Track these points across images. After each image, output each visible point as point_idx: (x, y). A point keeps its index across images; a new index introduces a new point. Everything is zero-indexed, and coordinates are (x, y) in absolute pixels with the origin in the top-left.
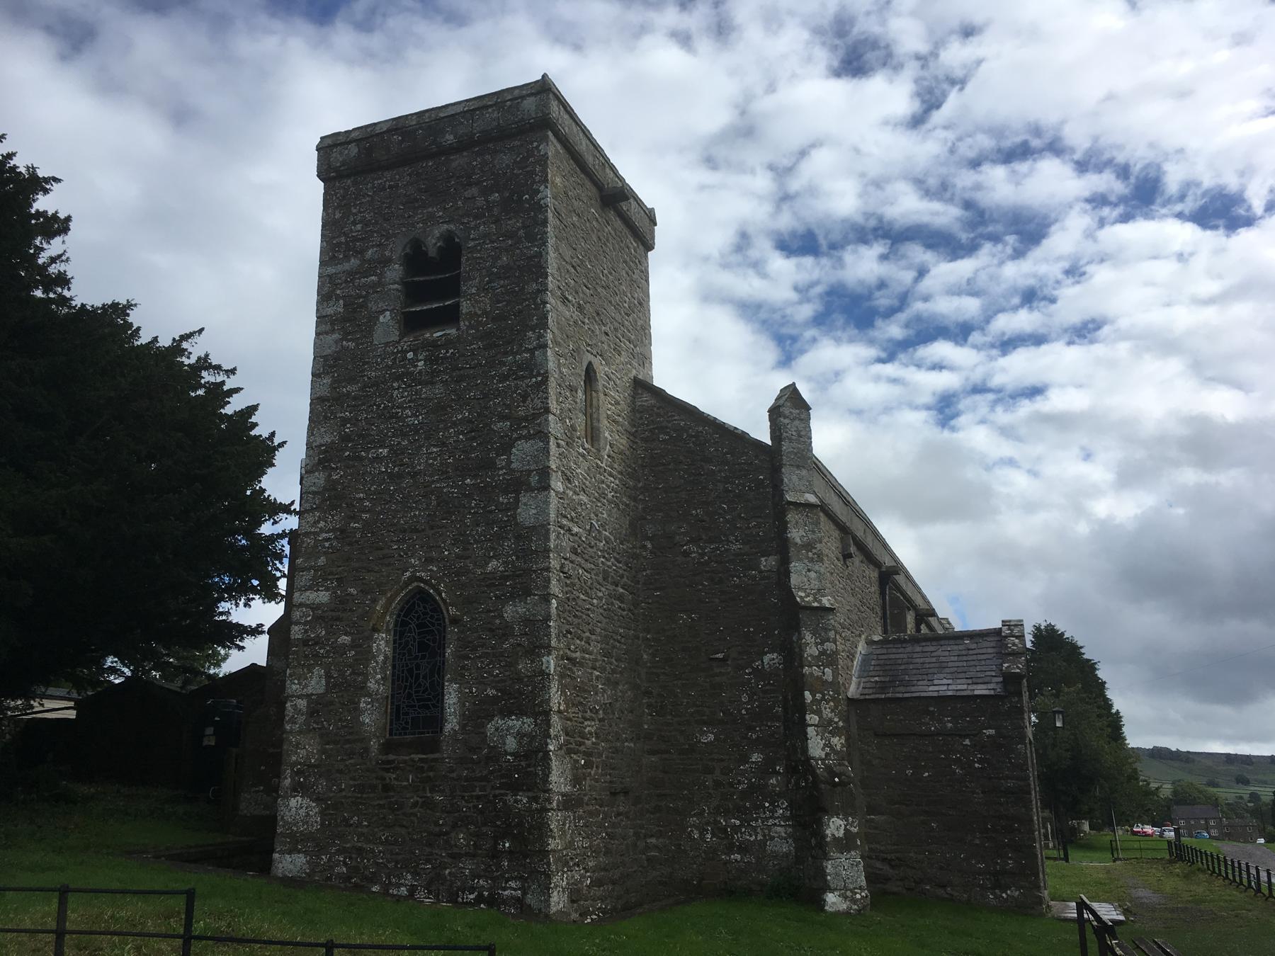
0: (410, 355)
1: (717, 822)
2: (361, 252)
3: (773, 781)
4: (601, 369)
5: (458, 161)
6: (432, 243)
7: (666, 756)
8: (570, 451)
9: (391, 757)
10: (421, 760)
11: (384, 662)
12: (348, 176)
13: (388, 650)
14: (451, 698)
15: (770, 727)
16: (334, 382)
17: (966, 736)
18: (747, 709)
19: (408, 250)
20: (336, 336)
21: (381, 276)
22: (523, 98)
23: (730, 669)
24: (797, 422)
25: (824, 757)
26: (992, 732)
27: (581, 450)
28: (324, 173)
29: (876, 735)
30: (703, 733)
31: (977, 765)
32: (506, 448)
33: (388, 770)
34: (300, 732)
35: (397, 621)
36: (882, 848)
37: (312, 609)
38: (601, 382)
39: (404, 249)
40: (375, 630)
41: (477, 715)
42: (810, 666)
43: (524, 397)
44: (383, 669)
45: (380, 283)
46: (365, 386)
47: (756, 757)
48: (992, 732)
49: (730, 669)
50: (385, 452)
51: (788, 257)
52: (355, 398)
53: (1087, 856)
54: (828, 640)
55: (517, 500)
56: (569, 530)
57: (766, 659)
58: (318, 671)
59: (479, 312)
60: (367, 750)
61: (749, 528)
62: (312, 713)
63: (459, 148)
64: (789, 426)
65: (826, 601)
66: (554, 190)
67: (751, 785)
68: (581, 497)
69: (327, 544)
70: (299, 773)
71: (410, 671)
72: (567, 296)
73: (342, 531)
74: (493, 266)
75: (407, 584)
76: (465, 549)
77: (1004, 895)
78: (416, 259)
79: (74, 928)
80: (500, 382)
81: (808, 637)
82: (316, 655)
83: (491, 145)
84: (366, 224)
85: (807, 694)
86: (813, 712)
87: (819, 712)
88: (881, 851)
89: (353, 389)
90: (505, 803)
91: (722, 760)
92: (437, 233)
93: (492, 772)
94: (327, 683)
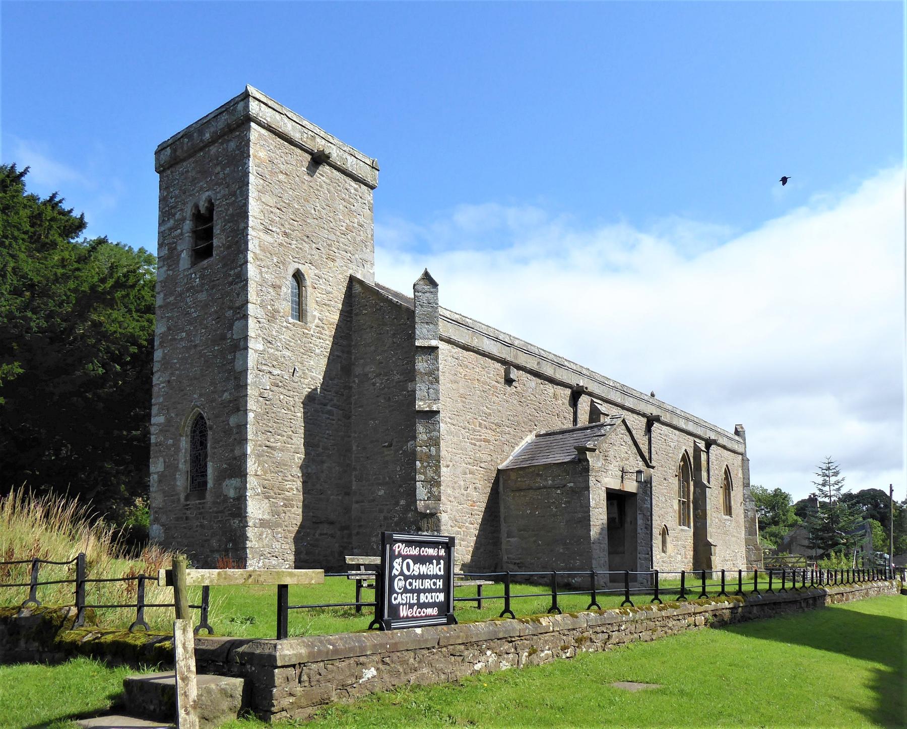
0: (193, 276)
2: (174, 215)
4: (309, 272)
5: (213, 150)
7: (362, 504)
8: (271, 325)
9: (188, 503)
10: (200, 504)
11: (185, 453)
12: (168, 168)
13: (188, 446)
14: (210, 471)
15: (409, 484)
16: (165, 295)
17: (558, 488)
18: (399, 475)
19: (193, 211)
20: (165, 268)
21: (182, 229)
22: (237, 103)
23: (392, 452)
24: (428, 295)
25: (426, 499)
26: (572, 484)
27: (285, 324)
28: (161, 169)
30: (379, 490)
31: (563, 505)
32: (231, 327)
33: (187, 509)
34: (155, 492)
35: (191, 430)
36: (514, 557)
37: (159, 426)
38: (308, 282)
39: (191, 211)
40: (181, 436)
42: (421, 447)
43: (238, 295)
44: (185, 457)
45: (182, 234)
46: (176, 297)
47: (402, 502)
48: (572, 484)
49: (392, 452)
50: (184, 334)
52: (173, 305)
54: (434, 430)
55: (235, 356)
57: (409, 444)
58: (161, 459)
59: (221, 245)
60: (179, 500)
61: (403, 365)
62: (160, 481)
63: (212, 142)
64: (421, 297)
66: (257, 160)
67: (400, 517)
68: (284, 353)
69: (163, 390)
70: (156, 512)
71: (197, 457)
72: (270, 228)
73: (169, 382)
74: (226, 215)
76: (215, 387)
77: (573, 581)
80: (229, 287)
81: (420, 428)
82: (160, 451)
83: (226, 137)
84: (176, 197)
85: (418, 463)
88: (514, 559)
89: (172, 298)
90: (230, 524)
91: (387, 505)
92: (204, 198)
93: (225, 508)
94: (165, 465)
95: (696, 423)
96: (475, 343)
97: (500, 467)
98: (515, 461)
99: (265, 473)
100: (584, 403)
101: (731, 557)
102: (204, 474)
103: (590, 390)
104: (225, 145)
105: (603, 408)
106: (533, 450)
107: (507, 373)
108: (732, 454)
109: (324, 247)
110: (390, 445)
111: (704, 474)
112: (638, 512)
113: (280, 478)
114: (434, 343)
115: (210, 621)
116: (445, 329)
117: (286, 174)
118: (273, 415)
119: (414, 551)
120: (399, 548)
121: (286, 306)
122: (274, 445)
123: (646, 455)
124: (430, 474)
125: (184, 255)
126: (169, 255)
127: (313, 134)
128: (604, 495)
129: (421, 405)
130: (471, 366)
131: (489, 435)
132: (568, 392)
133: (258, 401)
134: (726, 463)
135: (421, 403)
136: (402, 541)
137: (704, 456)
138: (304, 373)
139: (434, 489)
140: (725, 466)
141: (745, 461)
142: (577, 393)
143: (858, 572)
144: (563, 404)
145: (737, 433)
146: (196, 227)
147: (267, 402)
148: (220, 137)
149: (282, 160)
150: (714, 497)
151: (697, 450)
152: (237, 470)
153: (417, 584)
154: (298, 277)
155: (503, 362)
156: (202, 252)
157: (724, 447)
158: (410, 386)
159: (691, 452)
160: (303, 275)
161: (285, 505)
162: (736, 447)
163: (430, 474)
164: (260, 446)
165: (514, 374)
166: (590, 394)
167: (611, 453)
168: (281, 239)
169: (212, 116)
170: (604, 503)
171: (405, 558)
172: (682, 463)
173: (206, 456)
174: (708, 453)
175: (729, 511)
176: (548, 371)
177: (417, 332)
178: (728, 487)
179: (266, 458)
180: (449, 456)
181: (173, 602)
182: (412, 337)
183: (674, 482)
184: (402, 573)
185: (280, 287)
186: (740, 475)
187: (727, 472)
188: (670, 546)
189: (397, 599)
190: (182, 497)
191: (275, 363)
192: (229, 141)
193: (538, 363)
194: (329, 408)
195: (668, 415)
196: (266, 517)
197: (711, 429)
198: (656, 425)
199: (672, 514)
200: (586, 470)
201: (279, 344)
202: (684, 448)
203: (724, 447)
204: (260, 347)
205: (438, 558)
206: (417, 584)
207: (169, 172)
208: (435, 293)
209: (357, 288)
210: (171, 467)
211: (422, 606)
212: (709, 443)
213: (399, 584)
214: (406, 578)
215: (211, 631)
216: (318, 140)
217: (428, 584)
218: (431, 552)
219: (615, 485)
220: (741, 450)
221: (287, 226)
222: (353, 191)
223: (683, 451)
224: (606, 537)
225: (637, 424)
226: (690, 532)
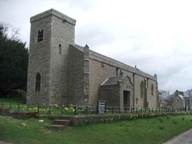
6: (40, 30)
41: (43, 88)
56: (54, 65)
63: (43, 18)
65: (88, 73)
78: (39, 32)
87: (86, 87)
96: (96, 59)
98: (104, 84)
100: (119, 70)
101: (36, 101)
102: (39, 86)
103: (120, 67)
107: (103, 64)
108: (154, 81)
111: (147, 86)
114: (88, 59)
116: (91, 57)
119: (101, 103)
120: (99, 103)
123: (133, 83)
124: (87, 87)
125: (36, 40)
126: (32, 39)
129: (85, 73)
131: (99, 78)
132: (115, 68)
137: (146, 82)
139: (88, 90)
141: (157, 83)
142: (117, 69)
143: (180, 109)
150: (149, 92)
151: (145, 80)
153: (101, 108)
154: (60, 45)
155: (102, 62)
157: (152, 79)
159: (143, 81)
162: (154, 79)
163: (87, 87)
165: (104, 65)
166: (120, 68)
167: (125, 82)
168: (57, 38)
169: (43, 13)
175: (152, 94)
178: (152, 89)
180: (90, 83)
186: (155, 85)
187: (152, 85)
188: (138, 103)
189: (99, 110)
190: (35, 91)
198: (135, 75)
199: (139, 95)
200: (119, 86)
203: (152, 79)
206: (101, 108)
209: (71, 47)
211: (102, 111)
212: (148, 79)
213: (99, 108)
214: (100, 107)
216: (64, 17)
217: (103, 108)
218: (103, 103)
219: (126, 89)
220: (156, 80)
225: (130, 75)
226: (143, 99)
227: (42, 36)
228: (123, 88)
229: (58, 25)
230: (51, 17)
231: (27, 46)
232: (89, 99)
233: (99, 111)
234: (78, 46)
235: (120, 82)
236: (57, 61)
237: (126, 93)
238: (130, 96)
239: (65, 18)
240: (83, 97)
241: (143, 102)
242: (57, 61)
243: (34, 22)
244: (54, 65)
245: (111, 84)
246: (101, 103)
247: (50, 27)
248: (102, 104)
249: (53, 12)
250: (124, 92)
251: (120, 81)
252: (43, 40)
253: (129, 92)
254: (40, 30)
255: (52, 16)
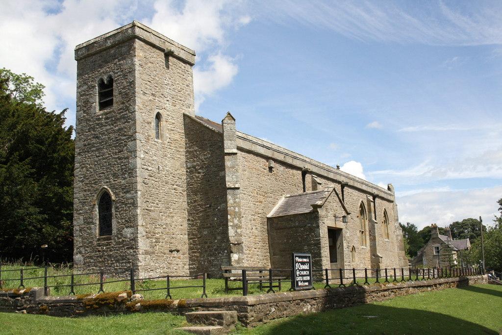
1: (208, 259)
3: (223, 245)
6: (105, 78)
10: (107, 243)
17: (302, 227)
24: (229, 125)
26: (310, 225)
28: (78, 59)
29: (276, 229)
47: (219, 238)
48: (310, 225)
51: (56, 14)
53: (166, 273)
56: (147, 169)
75: (102, 190)
78: (102, 84)
79: (172, 287)
83: (120, 45)
86: (231, 222)
95: (367, 185)
97: (269, 216)
99: (147, 224)
100: (308, 177)
102: (110, 226)
104: (120, 49)
105: (318, 180)
106: (287, 205)
109: (171, 99)
110: (210, 206)
111: (373, 215)
112: (344, 239)
113: (153, 227)
115: (206, 292)
117: (152, 63)
118: (149, 192)
119: (300, 260)
120: (297, 259)
121: (153, 133)
122: (150, 208)
126: (83, 104)
127: (164, 41)
128: (326, 230)
130: (251, 161)
131: (261, 198)
133: (142, 185)
134: (384, 208)
135: (229, 183)
136: (298, 256)
137: (372, 204)
138: (163, 168)
139: (239, 231)
140: (384, 210)
142: (305, 172)
144: (298, 179)
145: (389, 189)
146: (101, 90)
147: (147, 186)
148: (117, 45)
149: (150, 56)
150: (379, 228)
151: (369, 201)
152: (131, 222)
153: (302, 273)
154: (158, 116)
155: (267, 158)
156: (106, 102)
158: (221, 174)
160: (161, 115)
161: (156, 242)
163: (236, 221)
164: (144, 209)
166: (311, 173)
168: (151, 98)
170: (327, 235)
171: (299, 262)
172: (360, 209)
173: (111, 215)
174: (374, 202)
176: (289, 161)
177: (225, 145)
179: (147, 216)
181: (308, 268)
182: (222, 147)
183: (357, 220)
184: (298, 269)
185: (151, 123)
189: (299, 279)
191: (149, 164)
192: (122, 47)
193: (284, 157)
194: (175, 186)
195: (352, 181)
196: (148, 249)
197: (375, 188)
201: (151, 153)
202: (361, 200)
204: (142, 156)
205: (307, 262)
206: (302, 273)
207: (84, 60)
208: (234, 124)
210: (88, 222)
212: (375, 197)
213: (298, 273)
215: (206, 297)
216: (166, 43)
218: (305, 260)
219: (332, 225)
221: (153, 90)
222: (183, 68)
223: (361, 201)
224: (329, 254)
227: (111, 93)
228: (327, 221)
229: (150, 65)
230: (134, 42)
231: (70, 121)
232: (242, 253)
233: (297, 282)
234: (208, 121)
235: (320, 206)
236: (155, 158)
237: (335, 234)
238: (344, 242)
239: (167, 47)
240: (225, 249)
241: (368, 255)
242: (155, 158)
243: (85, 57)
244: (147, 169)
245: (296, 212)
246: (300, 260)
247: (132, 71)
248: (303, 263)
249: (138, 32)
250: (328, 230)
251: (319, 203)
252: (115, 105)
253: (341, 229)
254: (105, 78)
255: (136, 40)
